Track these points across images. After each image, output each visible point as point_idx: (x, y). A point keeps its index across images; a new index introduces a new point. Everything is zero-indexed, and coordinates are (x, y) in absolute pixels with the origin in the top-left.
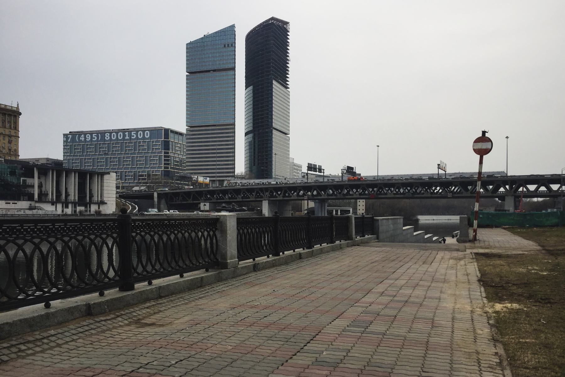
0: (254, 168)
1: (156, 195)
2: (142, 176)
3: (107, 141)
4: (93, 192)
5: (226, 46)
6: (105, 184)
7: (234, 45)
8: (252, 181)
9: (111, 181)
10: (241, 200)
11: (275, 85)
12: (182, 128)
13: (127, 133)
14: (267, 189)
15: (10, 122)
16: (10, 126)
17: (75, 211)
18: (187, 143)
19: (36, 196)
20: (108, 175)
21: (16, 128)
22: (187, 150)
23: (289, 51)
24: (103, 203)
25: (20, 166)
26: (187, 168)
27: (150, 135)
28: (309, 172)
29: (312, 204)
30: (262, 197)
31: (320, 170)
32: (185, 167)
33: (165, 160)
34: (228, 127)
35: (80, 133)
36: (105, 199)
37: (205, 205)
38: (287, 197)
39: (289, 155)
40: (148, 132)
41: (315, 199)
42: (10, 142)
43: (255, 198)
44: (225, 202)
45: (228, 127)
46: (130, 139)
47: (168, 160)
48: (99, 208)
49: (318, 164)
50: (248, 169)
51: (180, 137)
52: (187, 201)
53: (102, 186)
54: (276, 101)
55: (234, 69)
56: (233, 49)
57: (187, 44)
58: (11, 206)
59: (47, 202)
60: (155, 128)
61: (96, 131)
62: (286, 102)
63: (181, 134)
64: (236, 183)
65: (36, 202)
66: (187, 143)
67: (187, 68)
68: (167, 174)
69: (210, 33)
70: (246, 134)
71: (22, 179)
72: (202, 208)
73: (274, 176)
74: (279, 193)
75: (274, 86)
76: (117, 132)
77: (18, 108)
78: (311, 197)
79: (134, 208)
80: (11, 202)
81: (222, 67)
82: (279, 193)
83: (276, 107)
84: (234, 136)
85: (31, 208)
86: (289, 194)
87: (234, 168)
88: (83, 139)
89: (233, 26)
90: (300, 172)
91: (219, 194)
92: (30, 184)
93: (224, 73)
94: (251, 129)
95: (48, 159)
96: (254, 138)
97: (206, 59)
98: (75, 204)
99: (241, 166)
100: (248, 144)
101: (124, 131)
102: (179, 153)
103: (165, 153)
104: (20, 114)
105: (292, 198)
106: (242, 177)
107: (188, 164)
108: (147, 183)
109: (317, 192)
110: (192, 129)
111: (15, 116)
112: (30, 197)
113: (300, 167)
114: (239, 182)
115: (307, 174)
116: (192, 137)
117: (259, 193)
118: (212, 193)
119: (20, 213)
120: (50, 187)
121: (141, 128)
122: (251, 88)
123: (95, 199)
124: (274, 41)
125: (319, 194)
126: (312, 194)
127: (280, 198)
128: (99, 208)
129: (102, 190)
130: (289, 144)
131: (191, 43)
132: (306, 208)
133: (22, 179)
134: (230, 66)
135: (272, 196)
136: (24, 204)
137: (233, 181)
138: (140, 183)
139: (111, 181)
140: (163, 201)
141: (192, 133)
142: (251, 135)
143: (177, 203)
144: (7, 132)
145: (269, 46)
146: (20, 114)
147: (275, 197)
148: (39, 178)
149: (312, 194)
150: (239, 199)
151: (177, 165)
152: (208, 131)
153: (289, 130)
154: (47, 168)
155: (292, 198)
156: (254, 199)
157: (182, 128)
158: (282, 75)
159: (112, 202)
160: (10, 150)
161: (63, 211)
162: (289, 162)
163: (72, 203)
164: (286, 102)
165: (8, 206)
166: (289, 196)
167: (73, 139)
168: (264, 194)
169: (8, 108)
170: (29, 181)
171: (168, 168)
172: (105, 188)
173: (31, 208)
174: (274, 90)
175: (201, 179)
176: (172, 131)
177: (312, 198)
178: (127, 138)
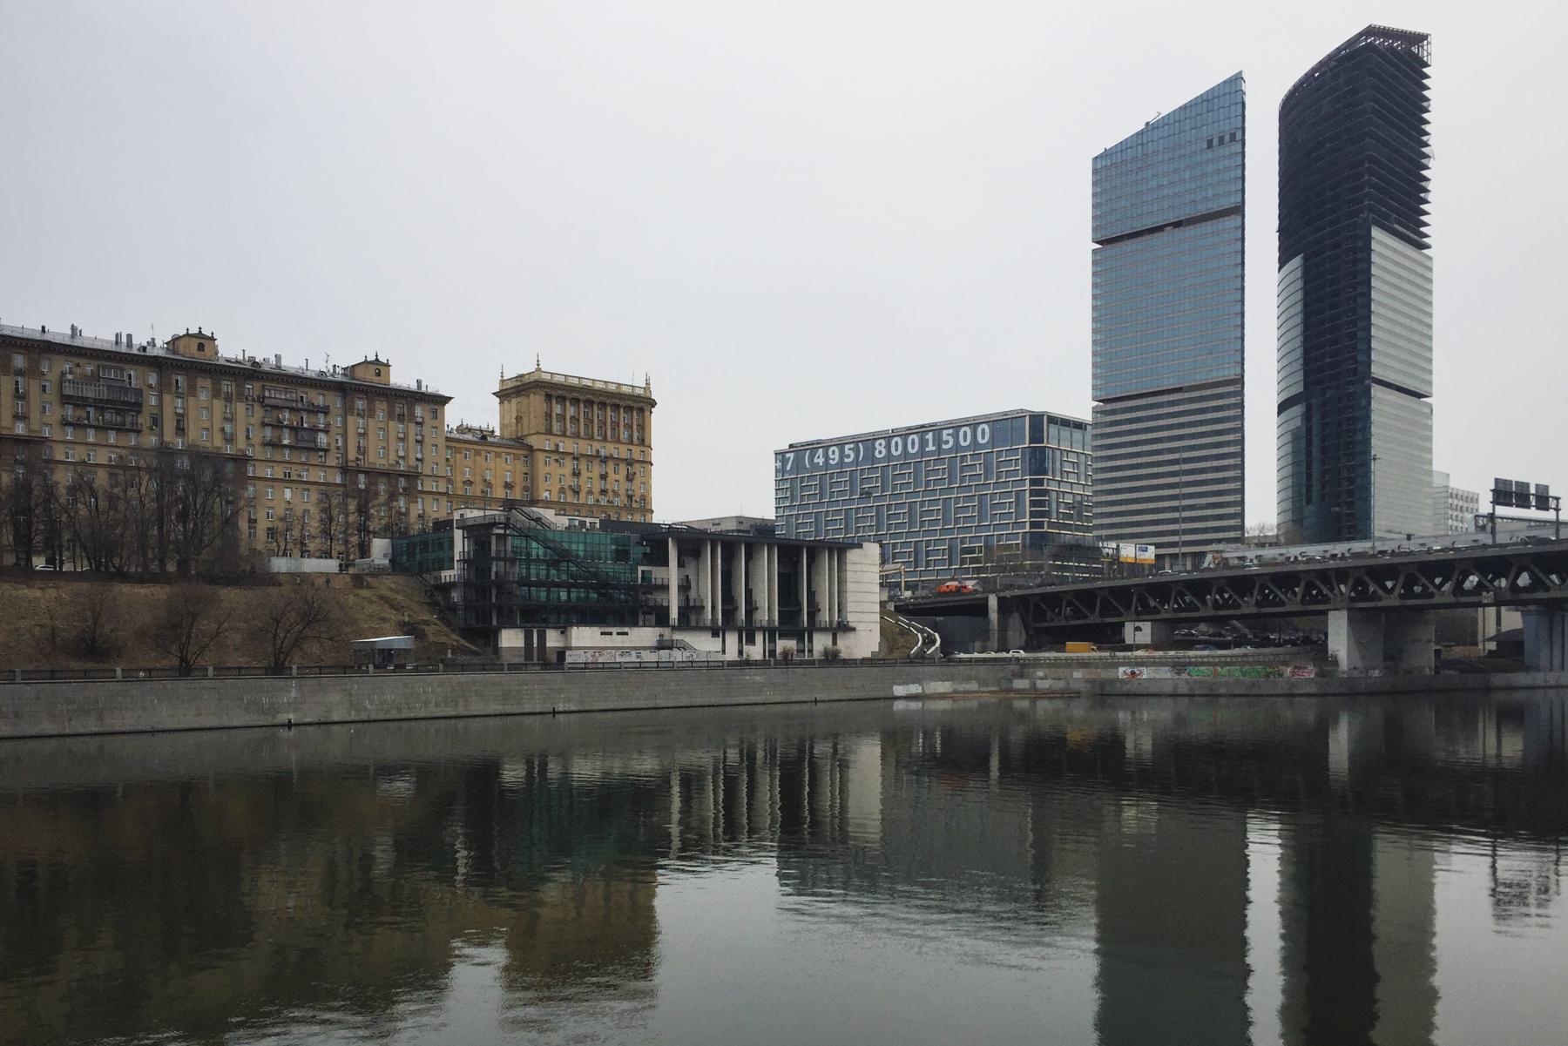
0: (1310, 510)
1: (993, 602)
2: (972, 550)
3: (880, 461)
4: (755, 596)
5: (1215, 142)
6: (850, 576)
7: (1239, 137)
8: (1294, 551)
9: (866, 568)
10: (1254, 610)
11: (1380, 242)
12: (1079, 404)
13: (930, 436)
14: (1342, 575)
15: (629, 427)
16: (631, 436)
17: (773, 653)
18: (1095, 448)
19: (674, 614)
20: (857, 551)
21: (644, 442)
22: (1096, 471)
23: (1427, 128)
24: (844, 628)
25: (635, 537)
26: (1096, 522)
27: (992, 436)
28: (1501, 511)
29: (1513, 620)
30: (1326, 600)
31: (1543, 500)
32: (1088, 519)
33: (1033, 504)
34: (1220, 390)
35: (813, 447)
36: (851, 619)
37: (1138, 629)
38: (1417, 596)
39: (1430, 462)
40: (985, 426)
41: (1525, 603)
42: (630, 478)
43: (1303, 601)
44: (1238, 618)
45: (1220, 390)
46: (939, 450)
47: (1041, 503)
48: (835, 643)
49: (1533, 479)
50: (1289, 516)
51: (1077, 434)
52: (1086, 617)
53: (842, 581)
54: (1385, 306)
55: (1239, 210)
56: (1237, 148)
57: (1095, 159)
58: (616, 641)
59: (700, 628)
60: (1006, 414)
61: (853, 437)
62: (1420, 293)
63: (1079, 426)
64: (1242, 558)
65: (674, 628)
66: (1095, 448)
67: (1095, 229)
68: (1038, 541)
69: (1164, 113)
70: (1282, 408)
71: (640, 569)
72: (1129, 641)
73: (1377, 534)
74: (1389, 584)
75: (1374, 245)
76: (905, 433)
77: (647, 388)
78: (1508, 596)
79: (929, 641)
80: (614, 630)
81: (1214, 207)
82: (1389, 584)
83: (1382, 311)
84: (1241, 417)
85: (662, 645)
86: (1425, 588)
87: (1242, 515)
88: (821, 461)
89: (1238, 78)
90: (1469, 516)
91: (1182, 595)
92: (659, 582)
93: (1207, 227)
94: (1299, 388)
95: (740, 520)
96: (1307, 417)
97: (1153, 200)
98: (771, 633)
99: (1264, 503)
100: (1289, 437)
101: (922, 430)
102: (1072, 482)
103: (1033, 482)
104: (653, 404)
105: (1433, 601)
106: (1262, 543)
107: (1099, 510)
108: (984, 570)
109: (1532, 575)
110: (1109, 407)
111: (641, 410)
112: (661, 618)
113: (1474, 499)
114: (1251, 554)
115: (1492, 517)
116: (1109, 430)
117: (1316, 586)
118: (1162, 591)
119: (627, 659)
120: (707, 590)
121: (967, 419)
122: (1297, 262)
123: (824, 617)
124: (1377, 101)
125: (1537, 584)
126: (1513, 587)
127: (1393, 601)
128: (835, 643)
129: (842, 592)
130: (1430, 428)
131: (1107, 154)
132: (1491, 631)
133: (640, 569)
134: (1227, 203)
135: (1363, 595)
136: (644, 635)
137: (1232, 553)
138: (967, 571)
139: (866, 568)
140: (1015, 620)
141: (1109, 418)
142: (1297, 410)
143: (1056, 623)
144: (623, 452)
145: (1360, 136)
146: (653, 404)
147: (1375, 597)
148: (681, 564)
149: (1513, 587)
150: (1249, 606)
151: (1070, 517)
152: (1162, 413)
153: (1430, 383)
154: (733, 544)
155: (1437, 600)
156: (1300, 608)
157: (1079, 404)
158: (1406, 212)
159: (871, 626)
160: (630, 497)
161: (740, 652)
162: (1430, 484)
163: (763, 629)
164: (1420, 293)
165: (618, 641)
166: (1426, 594)
167: (798, 461)
168: (1332, 590)
169: (625, 390)
170: (657, 573)
171: (1041, 525)
172: (850, 586)
173: (662, 645)
174: (1374, 258)
175: (1128, 551)
176: (1053, 420)
177: (1514, 598)
178: (931, 448)
